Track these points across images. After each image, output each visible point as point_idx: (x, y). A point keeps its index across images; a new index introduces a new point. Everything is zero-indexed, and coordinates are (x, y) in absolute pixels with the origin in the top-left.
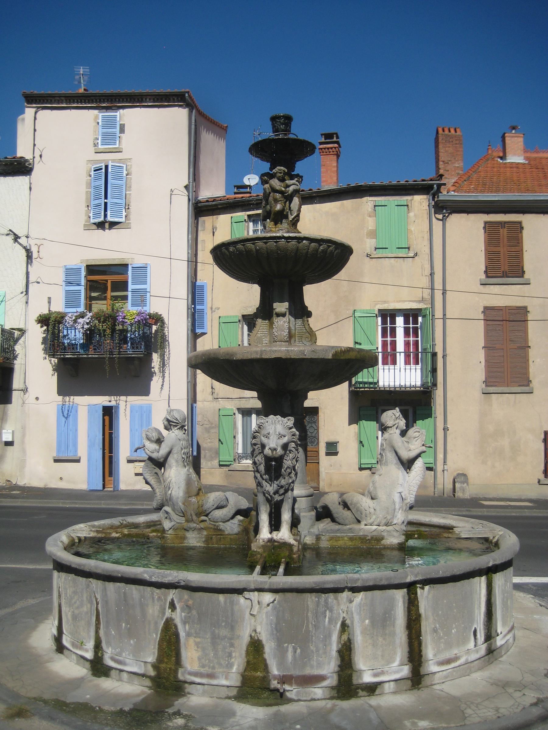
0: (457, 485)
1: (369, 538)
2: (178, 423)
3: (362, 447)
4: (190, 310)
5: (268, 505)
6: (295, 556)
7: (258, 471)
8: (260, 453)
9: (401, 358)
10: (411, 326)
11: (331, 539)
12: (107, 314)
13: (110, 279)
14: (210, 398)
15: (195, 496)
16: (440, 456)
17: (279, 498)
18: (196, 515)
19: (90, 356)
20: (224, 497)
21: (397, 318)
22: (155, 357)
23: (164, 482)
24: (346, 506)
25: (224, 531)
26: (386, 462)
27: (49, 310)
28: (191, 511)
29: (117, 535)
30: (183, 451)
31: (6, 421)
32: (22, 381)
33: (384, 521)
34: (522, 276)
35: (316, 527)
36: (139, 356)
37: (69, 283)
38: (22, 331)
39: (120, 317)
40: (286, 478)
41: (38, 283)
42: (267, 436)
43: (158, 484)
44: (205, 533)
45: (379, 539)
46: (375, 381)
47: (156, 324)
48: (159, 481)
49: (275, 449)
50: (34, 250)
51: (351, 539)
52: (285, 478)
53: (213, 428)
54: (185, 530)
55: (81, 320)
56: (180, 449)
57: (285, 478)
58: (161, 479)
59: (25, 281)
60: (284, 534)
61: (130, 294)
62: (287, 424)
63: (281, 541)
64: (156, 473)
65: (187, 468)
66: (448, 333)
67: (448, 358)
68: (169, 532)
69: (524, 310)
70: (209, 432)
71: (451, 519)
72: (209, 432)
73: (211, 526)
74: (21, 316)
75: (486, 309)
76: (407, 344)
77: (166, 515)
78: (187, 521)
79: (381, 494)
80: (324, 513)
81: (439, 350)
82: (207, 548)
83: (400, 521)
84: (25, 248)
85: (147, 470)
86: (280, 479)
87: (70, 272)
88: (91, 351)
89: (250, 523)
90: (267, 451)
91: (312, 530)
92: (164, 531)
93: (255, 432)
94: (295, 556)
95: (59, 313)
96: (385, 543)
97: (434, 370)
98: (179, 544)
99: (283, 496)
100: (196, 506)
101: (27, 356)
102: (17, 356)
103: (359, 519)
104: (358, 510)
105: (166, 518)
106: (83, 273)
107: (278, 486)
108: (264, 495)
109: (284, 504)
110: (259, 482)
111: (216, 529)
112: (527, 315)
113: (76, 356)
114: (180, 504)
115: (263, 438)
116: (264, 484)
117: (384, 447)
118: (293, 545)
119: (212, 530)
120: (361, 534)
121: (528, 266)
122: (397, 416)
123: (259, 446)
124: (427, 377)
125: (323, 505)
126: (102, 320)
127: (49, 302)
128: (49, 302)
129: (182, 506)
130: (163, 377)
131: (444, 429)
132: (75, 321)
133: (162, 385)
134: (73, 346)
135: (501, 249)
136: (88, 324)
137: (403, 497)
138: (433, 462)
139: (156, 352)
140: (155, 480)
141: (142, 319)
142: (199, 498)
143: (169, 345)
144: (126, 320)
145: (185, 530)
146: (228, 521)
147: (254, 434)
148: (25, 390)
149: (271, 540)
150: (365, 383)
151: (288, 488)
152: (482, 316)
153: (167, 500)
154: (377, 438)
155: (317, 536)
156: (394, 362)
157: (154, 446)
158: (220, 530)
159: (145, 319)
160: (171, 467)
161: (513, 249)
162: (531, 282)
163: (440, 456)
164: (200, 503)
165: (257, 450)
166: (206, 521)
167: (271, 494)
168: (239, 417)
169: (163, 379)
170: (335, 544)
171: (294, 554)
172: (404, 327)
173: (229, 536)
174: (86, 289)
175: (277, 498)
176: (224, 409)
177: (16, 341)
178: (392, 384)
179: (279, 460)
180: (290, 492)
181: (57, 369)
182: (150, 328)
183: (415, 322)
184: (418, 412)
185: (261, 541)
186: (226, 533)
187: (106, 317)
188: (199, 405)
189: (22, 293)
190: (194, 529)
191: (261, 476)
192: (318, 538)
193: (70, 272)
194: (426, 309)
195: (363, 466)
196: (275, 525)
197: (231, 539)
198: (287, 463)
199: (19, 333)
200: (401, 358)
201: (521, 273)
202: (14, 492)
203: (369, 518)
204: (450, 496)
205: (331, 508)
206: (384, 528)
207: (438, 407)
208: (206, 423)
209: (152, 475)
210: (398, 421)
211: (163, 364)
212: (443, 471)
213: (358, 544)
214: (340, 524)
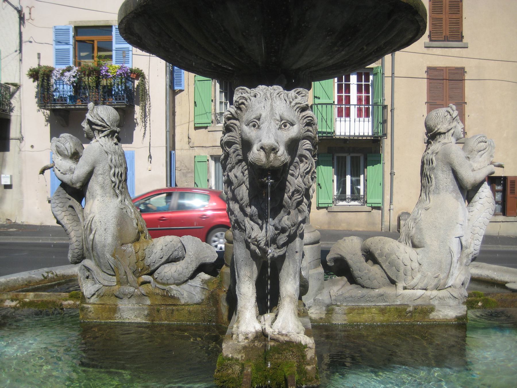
0: (402, 222)
1: (411, 309)
2: (104, 127)
3: (319, 189)
4: (168, 68)
5: (255, 267)
6: (309, 368)
7: (235, 199)
8: (240, 161)
9: (353, 111)
10: (363, 83)
11: (351, 310)
12: (92, 68)
13: (97, 39)
14: (187, 146)
15: (133, 242)
16: (387, 197)
17: (278, 253)
18: (134, 273)
19: (77, 107)
20: (180, 245)
21: (351, 76)
22: (138, 109)
23: (84, 220)
24: (370, 256)
25: (178, 299)
26: (437, 188)
27: (39, 65)
28: (126, 267)
29: (13, 304)
30: (112, 171)
31: (5, 166)
32: (18, 131)
33: (434, 283)
34: (461, 41)
35: (325, 291)
36: (122, 106)
37: (58, 42)
38: (17, 86)
39: (104, 71)
40: (293, 212)
41: (31, 42)
42: (255, 124)
43: (75, 224)
44: (148, 302)
45: (425, 310)
46: (333, 131)
47: (138, 79)
48: (76, 219)
49: (274, 150)
50: (26, 11)
51: (382, 311)
52: (289, 213)
53: (189, 172)
54: (116, 297)
55: (67, 74)
56: (107, 167)
57: (289, 213)
58: (80, 216)
59: (18, 41)
60: (286, 323)
61: (114, 53)
62: (297, 101)
63: (282, 338)
64: (71, 207)
65: (120, 198)
66: (395, 89)
67: (396, 112)
68: (92, 301)
69: (462, 71)
70: (186, 176)
71: (489, 269)
72: (186, 176)
73: (157, 291)
74: (13, 72)
75: (430, 70)
76: (359, 99)
77: (87, 274)
78: (120, 283)
79: (430, 239)
80: (339, 268)
81: (388, 102)
82: (151, 327)
83: (459, 282)
84: (16, 9)
85: (57, 201)
86: (280, 215)
87: (59, 32)
88: (79, 103)
89: (220, 285)
90: (256, 154)
91: (319, 297)
92: (83, 298)
93: (229, 119)
94: (309, 368)
95: (47, 67)
96: (436, 317)
97: (385, 122)
98: (107, 319)
99: (285, 248)
100: (134, 259)
101: (22, 108)
102: (12, 109)
103: (394, 278)
104: (392, 264)
105: (87, 277)
106: (72, 34)
107: (276, 229)
108: (248, 247)
109: (286, 263)
110: (237, 221)
111: (164, 296)
112: (464, 75)
113: (64, 107)
114: (108, 256)
115: (245, 128)
116: (247, 225)
117: (434, 165)
118: (306, 346)
119: (159, 297)
120: (399, 303)
121: (466, 32)
122: (454, 116)
123: (238, 146)
124: (378, 127)
125: (336, 256)
126: (87, 73)
127: (39, 58)
128: (39, 58)
129: (111, 260)
130: (145, 126)
131: (391, 174)
132: (62, 74)
133: (145, 134)
134: (62, 99)
135: (443, 16)
136: (74, 77)
137: (464, 243)
138: (381, 202)
139: (138, 105)
140: (70, 217)
141: (124, 73)
142: (138, 245)
143: (149, 98)
144: (109, 74)
145: (116, 297)
146: (186, 282)
147: (228, 122)
148: (21, 139)
149: (262, 335)
150: (324, 133)
151: (295, 233)
152: (425, 76)
153: (88, 249)
154: (333, 181)
155: (328, 306)
156: (348, 115)
157: (67, 164)
158: (173, 297)
159: (127, 73)
160: (93, 197)
161: (454, 16)
162: (469, 46)
163: (387, 197)
164: (140, 253)
165: (233, 156)
166: (149, 282)
167: (262, 244)
168: (212, 163)
169: (145, 129)
170: (357, 319)
171: (308, 364)
172: (357, 84)
173: (187, 307)
174: (75, 48)
175: (272, 252)
176: (200, 156)
177: (12, 95)
178: (347, 134)
179: (280, 173)
180: (298, 239)
181: (50, 120)
182: (134, 82)
183: (367, 80)
184: (368, 159)
185: (241, 337)
186: (183, 302)
187: (91, 71)
188: (178, 153)
189: (16, 51)
190: (132, 296)
191: (242, 209)
192: (330, 310)
193: (59, 32)
194: (377, 67)
195: (320, 206)
196: (268, 300)
197: (190, 312)
198: (295, 182)
199: (15, 88)
200: (353, 111)
201: (460, 38)
202: (11, 230)
203: (410, 278)
204: (395, 232)
205: (350, 262)
206: (435, 293)
207: (386, 155)
208: (183, 168)
209: (65, 209)
210: (455, 123)
211: (145, 115)
212: (390, 210)
213: (395, 319)
214: (363, 287)
